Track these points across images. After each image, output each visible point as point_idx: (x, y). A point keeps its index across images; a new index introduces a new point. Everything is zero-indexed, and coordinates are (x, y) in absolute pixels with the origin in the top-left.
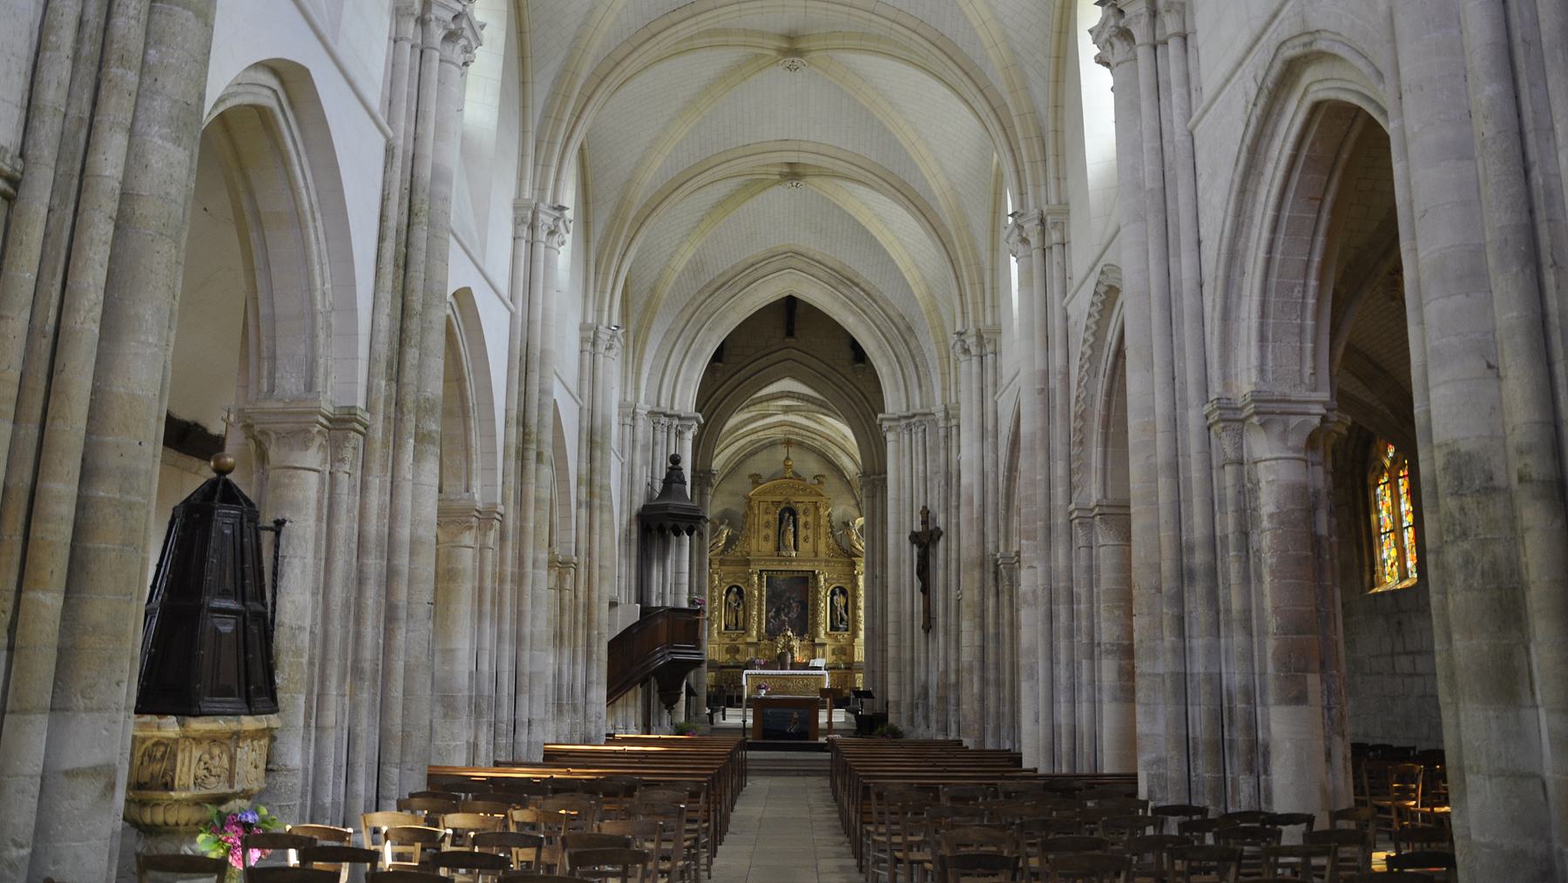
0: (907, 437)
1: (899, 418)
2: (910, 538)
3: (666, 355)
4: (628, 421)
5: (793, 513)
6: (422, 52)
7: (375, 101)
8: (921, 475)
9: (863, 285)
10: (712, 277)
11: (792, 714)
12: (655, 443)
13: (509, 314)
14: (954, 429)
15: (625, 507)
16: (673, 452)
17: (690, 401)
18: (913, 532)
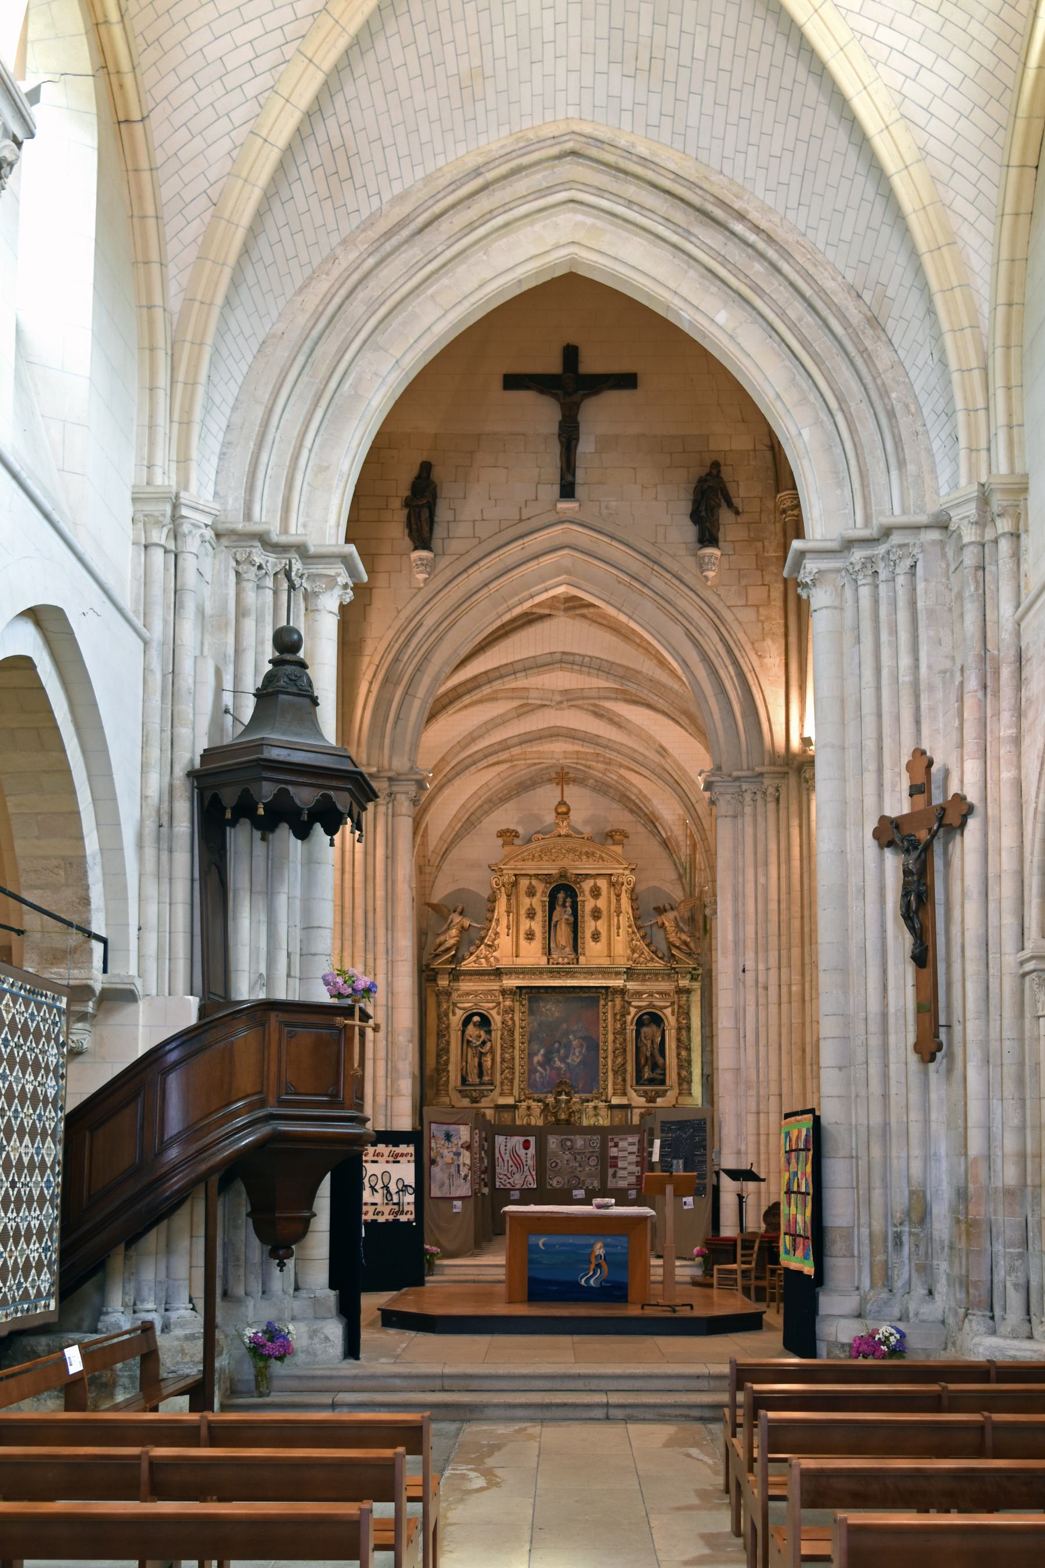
0: (865, 592)
1: (849, 544)
2: (877, 834)
3: (265, 396)
4: (159, 536)
5: (572, 893)
6: (176, 556)
7: (127, 605)
8: (905, 678)
9: (754, 216)
10: (375, 202)
11: (592, 1246)
12: (241, 613)
13: (142, 644)
14: (1004, 546)
15: (155, 753)
16: (283, 623)
17: (332, 519)
18: (883, 819)
